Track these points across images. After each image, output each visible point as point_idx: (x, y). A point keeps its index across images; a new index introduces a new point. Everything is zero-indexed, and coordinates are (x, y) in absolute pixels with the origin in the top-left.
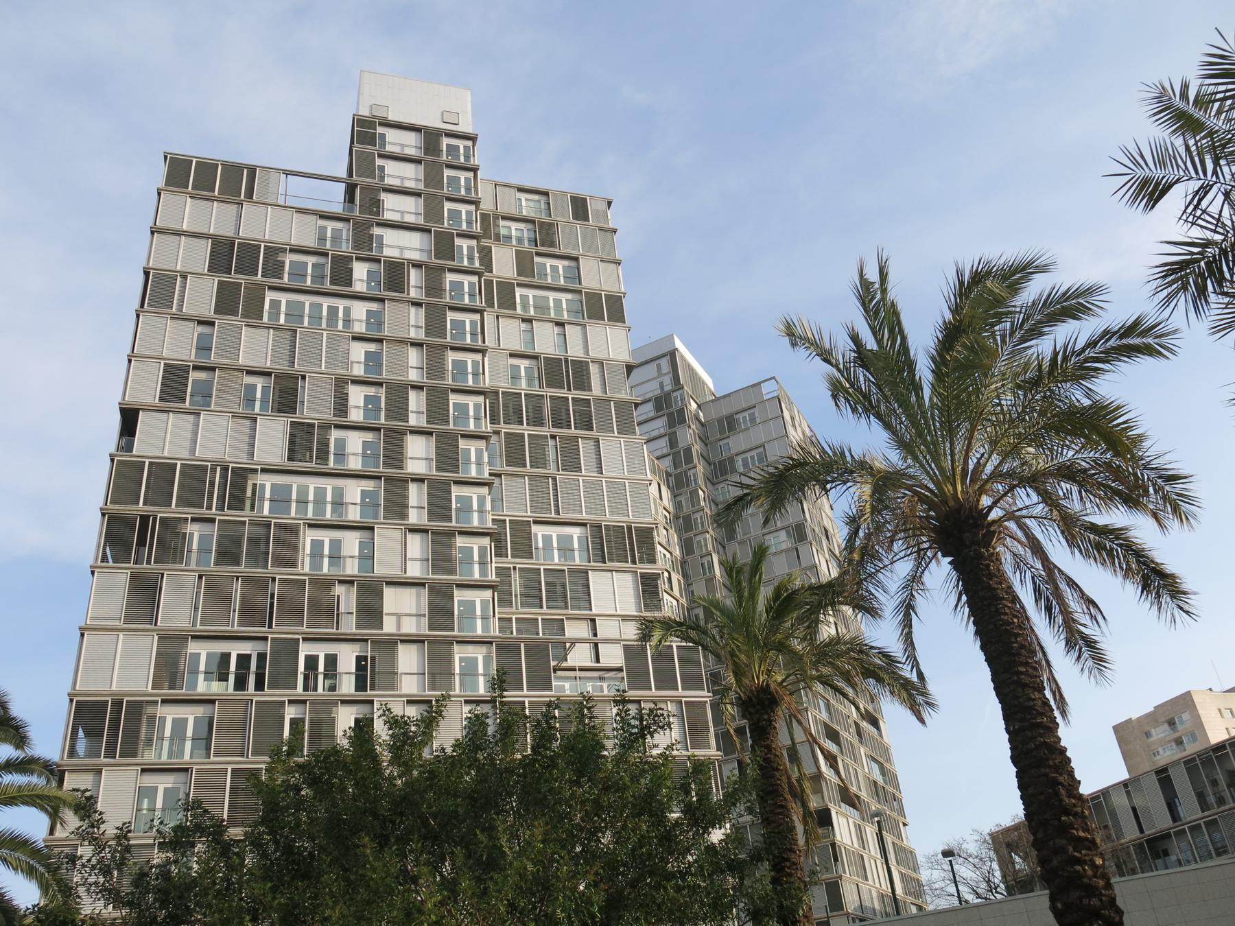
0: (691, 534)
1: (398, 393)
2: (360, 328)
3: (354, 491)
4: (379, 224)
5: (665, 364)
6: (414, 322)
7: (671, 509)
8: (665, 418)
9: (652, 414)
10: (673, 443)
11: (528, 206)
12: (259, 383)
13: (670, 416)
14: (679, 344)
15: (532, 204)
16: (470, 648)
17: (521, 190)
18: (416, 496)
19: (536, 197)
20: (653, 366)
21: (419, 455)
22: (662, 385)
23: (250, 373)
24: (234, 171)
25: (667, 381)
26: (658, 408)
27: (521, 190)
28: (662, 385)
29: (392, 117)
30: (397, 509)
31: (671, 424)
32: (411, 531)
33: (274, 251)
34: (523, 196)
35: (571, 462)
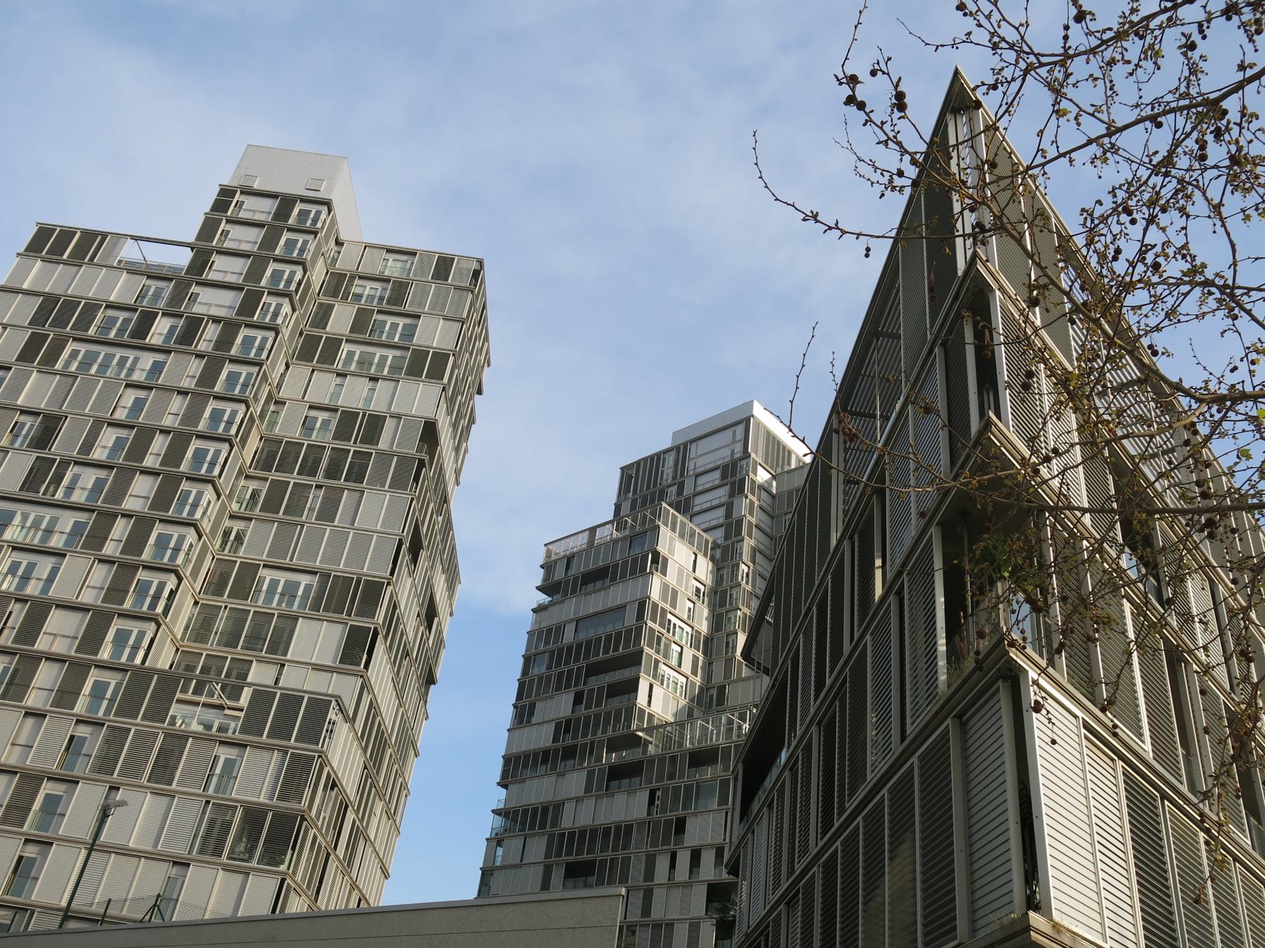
0: (723, 610)
1: (145, 436)
2: (138, 376)
3: (68, 521)
4: (197, 284)
5: (740, 430)
6: (189, 371)
7: (709, 582)
8: (728, 487)
9: (717, 482)
10: (729, 514)
11: (393, 268)
12: (28, 421)
13: (733, 484)
14: (759, 411)
15: (399, 265)
16: (107, 673)
17: (389, 251)
18: (120, 529)
19: (404, 258)
20: (729, 433)
21: (141, 491)
22: (733, 452)
23: (23, 412)
24: (90, 237)
25: (738, 448)
26: (724, 477)
27: (389, 251)
28: (733, 452)
29: (256, 186)
30: (97, 539)
31: (732, 495)
32: (100, 561)
33: (92, 308)
34: (391, 257)
35: (327, 513)
